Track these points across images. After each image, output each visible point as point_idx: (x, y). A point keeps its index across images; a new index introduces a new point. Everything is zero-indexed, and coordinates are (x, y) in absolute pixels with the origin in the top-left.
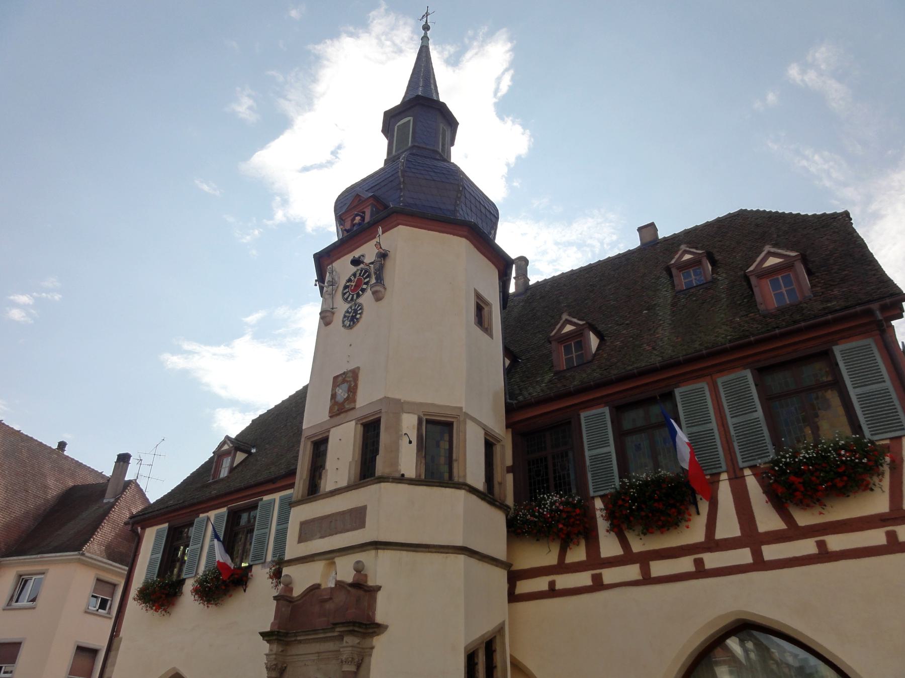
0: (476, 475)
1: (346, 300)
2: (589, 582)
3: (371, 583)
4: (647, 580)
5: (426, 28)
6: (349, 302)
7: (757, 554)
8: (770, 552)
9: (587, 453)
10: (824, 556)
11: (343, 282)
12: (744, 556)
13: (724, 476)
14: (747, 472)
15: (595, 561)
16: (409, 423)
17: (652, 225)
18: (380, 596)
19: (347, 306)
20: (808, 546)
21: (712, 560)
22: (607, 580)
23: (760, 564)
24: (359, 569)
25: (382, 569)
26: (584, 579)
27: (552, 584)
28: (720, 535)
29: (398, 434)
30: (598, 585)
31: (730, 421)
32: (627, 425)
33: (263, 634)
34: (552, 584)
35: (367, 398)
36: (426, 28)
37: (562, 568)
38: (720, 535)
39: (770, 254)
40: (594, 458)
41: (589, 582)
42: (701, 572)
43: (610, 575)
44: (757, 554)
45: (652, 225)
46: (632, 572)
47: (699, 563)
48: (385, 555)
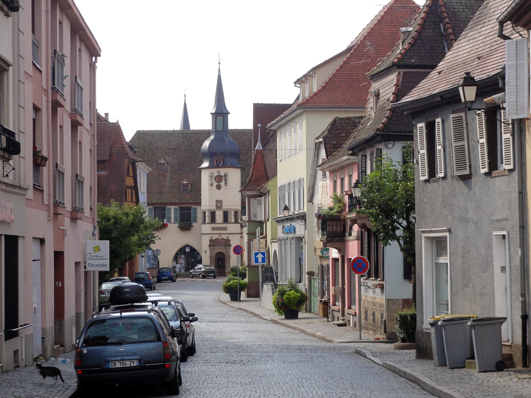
5: (219, 63)
24: (228, 237)
25: (231, 237)
35: (225, 207)
36: (219, 63)
48: (231, 235)
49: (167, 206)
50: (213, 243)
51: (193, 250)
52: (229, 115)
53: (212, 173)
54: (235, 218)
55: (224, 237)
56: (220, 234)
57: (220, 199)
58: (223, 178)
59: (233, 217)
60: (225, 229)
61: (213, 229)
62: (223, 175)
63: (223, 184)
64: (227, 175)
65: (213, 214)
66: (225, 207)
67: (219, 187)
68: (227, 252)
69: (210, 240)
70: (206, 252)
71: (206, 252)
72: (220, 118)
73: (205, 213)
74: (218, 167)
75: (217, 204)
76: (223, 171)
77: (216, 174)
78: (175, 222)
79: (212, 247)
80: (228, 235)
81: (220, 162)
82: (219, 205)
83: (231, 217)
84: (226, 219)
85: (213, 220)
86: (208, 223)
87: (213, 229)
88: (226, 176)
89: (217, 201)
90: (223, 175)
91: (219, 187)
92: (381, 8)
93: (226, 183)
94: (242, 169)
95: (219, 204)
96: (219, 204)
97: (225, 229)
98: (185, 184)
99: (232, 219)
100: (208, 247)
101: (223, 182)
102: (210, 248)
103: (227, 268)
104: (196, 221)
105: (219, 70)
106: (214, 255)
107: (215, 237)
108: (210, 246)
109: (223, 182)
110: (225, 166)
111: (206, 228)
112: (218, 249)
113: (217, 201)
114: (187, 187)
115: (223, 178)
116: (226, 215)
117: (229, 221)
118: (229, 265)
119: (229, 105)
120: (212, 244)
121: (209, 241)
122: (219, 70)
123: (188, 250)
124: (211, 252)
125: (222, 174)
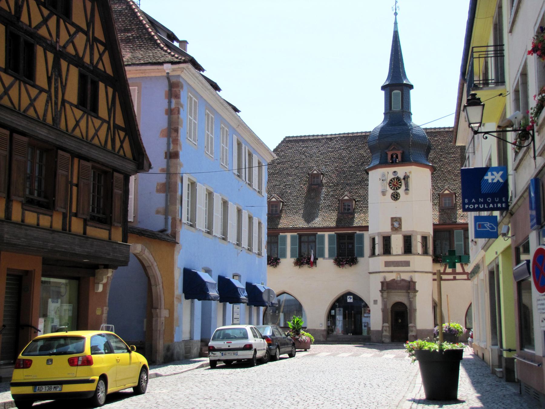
1: (391, 188)
2: (452, 278)
5: (396, 14)
9: (455, 243)
15: (454, 273)
16: (419, 239)
18: (417, 284)
19: (392, 191)
25: (417, 278)
26: (451, 277)
29: (416, 239)
30: (455, 279)
35: (406, 228)
36: (396, 14)
37: (444, 273)
40: (457, 245)
41: (452, 278)
43: (458, 277)
46: (465, 277)
48: (416, 274)
49: (319, 233)
50: (387, 287)
51: (357, 298)
52: (412, 92)
53: (384, 175)
54: (423, 246)
55: (406, 277)
56: (399, 272)
57: (398, 216)
58: (403, 181)
60: (407, 264)
62: (402, 177)
63: (401, 191)
64: (408, 177)
65: (387, 241)
66: (406, 228)
67: (396, 197)
68: (411, 303)
69: (382, 283)
70: (375, 302)
71: (375, 302)
72: (397, 92)
73: (374, 239)
74: (393, 163)
75: (392, 225)
76: (401, 171)
77: (391, 176)
78: (330, 256)
81: (397, 157)
82: (396, 225)
83: (416, 246)
84: (408, 249)
85: (387, 250)
86: (379, 255)
87: (387, 264)
88: (406, 178)
89: (392, 218)
90: (402, 177)
91: (396, 197)
92: (429, 204)
93: (407, 189)
94: (433, 169)
95: (396, 223)
96: (396, 223)
97: (407, 264)
98: (274, 202)
99: (418, 247)
100: (380, 294)
101: (403, 187)
102: (382, 296)
103: (410, 329)
104: (362, 255)
105: (396, 23)
106: (389, 307)
107: (390, 277)
109: (403, 187)
110: (405, 161)
111: (378, 263)
112: (399, 297)
113: (392, 218)
114: (276, 207)
115: (403, 181)
116: (408, 241)
118: (415, 323)
119: (412, 74)
122: (396, 23)
123: (350, 300)
125: (401, 175)
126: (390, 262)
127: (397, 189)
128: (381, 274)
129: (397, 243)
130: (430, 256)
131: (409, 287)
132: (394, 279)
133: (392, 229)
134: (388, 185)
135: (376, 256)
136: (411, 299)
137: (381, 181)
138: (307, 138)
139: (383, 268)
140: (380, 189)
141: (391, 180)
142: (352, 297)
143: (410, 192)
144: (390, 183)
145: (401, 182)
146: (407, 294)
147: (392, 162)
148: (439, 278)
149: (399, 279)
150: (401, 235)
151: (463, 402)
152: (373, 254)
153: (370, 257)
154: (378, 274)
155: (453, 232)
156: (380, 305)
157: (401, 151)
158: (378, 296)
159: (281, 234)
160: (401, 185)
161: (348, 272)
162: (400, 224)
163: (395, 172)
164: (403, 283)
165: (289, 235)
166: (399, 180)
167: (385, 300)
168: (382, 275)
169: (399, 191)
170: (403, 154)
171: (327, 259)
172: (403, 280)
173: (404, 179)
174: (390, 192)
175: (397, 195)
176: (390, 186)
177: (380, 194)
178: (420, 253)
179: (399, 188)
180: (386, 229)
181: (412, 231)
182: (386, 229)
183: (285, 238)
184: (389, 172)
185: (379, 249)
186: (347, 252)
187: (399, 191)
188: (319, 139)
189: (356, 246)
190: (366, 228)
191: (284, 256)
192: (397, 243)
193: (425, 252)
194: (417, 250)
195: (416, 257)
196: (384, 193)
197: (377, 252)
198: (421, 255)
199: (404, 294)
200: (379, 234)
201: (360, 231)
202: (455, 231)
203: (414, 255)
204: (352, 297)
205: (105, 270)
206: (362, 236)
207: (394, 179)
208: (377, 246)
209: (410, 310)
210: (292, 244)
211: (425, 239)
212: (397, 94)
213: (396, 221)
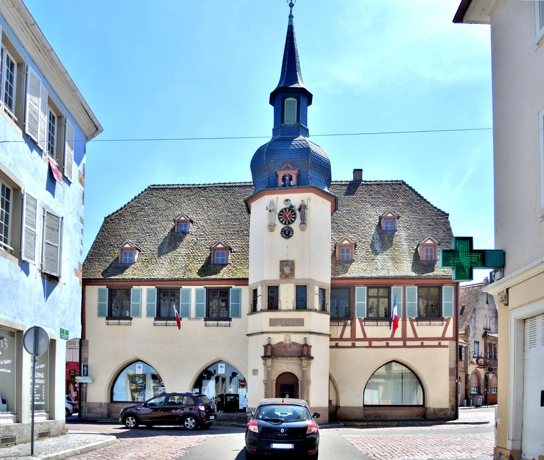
0: (317, 305)
1: (282, 222)
2: (351, 345)
3: (309, 345)
4: (370, 346)
6: (284, 224)
7: (405, 343)
8: (408, 343)
9: (356, 302)
10: (422, 346)
11: (278, 211)
12: (401, 343)
13: (401, 319)
14: (408, 319)
16: (317, 290)
17: (361, 170)
18: (312, 349)
20: (418, 343)
21: (391, 343)
22: (356, 345)
23: (405, 346)
25: (312, 340)
26: (349, 344)
27: (337, 344)
28: (395, 336)
29: (313, 290)
30: (354, 346)
31: (407, 302)
32: (370, 294)
33: (262, 357)
34: (337, 344)
35: (300, 275)
36: (291, 5)
38: (395, 336)
39: (430, 239)
41: (351, 345)
42: (387, 346)
43: (358, 344)
44: (405, 343)
45: (361, 170)
46: (366, 343)
47: (387, 344)
48: (313, 336)
49: (183, 287)
50: (271, 353)
53: (272, 203)
55: (298, 339)
57: (290, 258)
58: (298, 213)
59: (317, 298)
60: (301, 322)
61: (273, 322)
62: (297, 207)
63: (295, 226)
65: (273, 293)
66: (300, 275)
67: (287, 233)
68: (304, 373)
69: (266, 347)
70: (255, 372)
71: (255, 372)
72: (291, 101)
73: (255, 291)
75: (282, 270)
76: (296, 198)
77: (281, 206)
79: (269, 361)
80: (307, 336)
81: (291, 179)
82: (287, 270)
83: (313, 300)
84: (301, 304)
85: (273, 304)
86: (262, 311)
87: (273, 322)
88: (303, 208)
89: (281, 262)
91: (287, 233)
93: (303, 222)
95: (287, 268)
96: (287, 268)
99: (315, 301)
100: (261, 361)
101: (298, 220)
102: (265, 364)
105: (291, 17)
106: (274, 377)
107: (276, 339)
108: (265, 357)
109: (298, 220)
111: (263, 320)
113: (281, 262)
115: (298, 213)
116: (301, 292)
117: (309, 306)
120: (269, 354)
121: (263, 348)
122: (291, 17)
124: (268, 374)
126: (277, 319)
127: (289, 223)
128: (264, 335)
129: (287, 296)
130: (328, 314)
131: (304, 353)
132: (282, 343)
133: (281, 276)
134: (277, 215)
135: (259, 312)
136: (304, 369)
137: (268, 211)
138: (176, 186)
139: (266, 327)
140: (266, 222)
141: (282, 211)
142: (224, 365)
143: (308, 229)
144: (280, 215)
145: (295, 214)
146: (300, 361)
147: (284, 186)
148: (336, 344)
149: (288, 342)
150: (293, 285)
151: (53, 194)
152: (254, 310)
153: (249, 314)
154: (261, 336)
155: (354, 290)
156: (262, 375)
157: (296, 172)
158: (259, 364)
159: (134, 287)
160: (295, 218)
161: (217, 331)
162: (292, 270)
163: (287, 200)
164: (295, 348)
165: (145, 289)
166: (293, 211)
167: (270, 369)
168: (266, 336)
169: (292, 226)
170: (298, 176)
171: (193, 319)
172: (294, 344)
173: (300, 210)
174: (280, 226)
175: (289, 232)
176: (280, 218)
177: (266, 229)
178: (318, 309)
179: (293, 221)
180: (273, 275)
181: (309, 279)
182: (273, 275)
183: (139, 292)
184: (279, 200)
185: (262, 303)
186: (219, 306)
187: (292, 226)
188: (190, 188)
189: (231, 303)
190: (244, 281)
191: (138, 314)
192: (287, 296)
193: (323, 310)
194: (313, 305)
195: (313, 314)
196: (271, 228)
197: (259, 307)
198: (318, 312)
199: (296, 361)
200: (263, 282)
201: (236, 285)
202: (356, 288)
203: (310, 310)
204: (224, 365)
205: (207, 381)
206: (238, 292)
207: (285, 209)
208: (259, 299)
209: (301, 381)
210: (149, 300)
211: (323, 291)
212: (291, 103)
213: (287, 265)
